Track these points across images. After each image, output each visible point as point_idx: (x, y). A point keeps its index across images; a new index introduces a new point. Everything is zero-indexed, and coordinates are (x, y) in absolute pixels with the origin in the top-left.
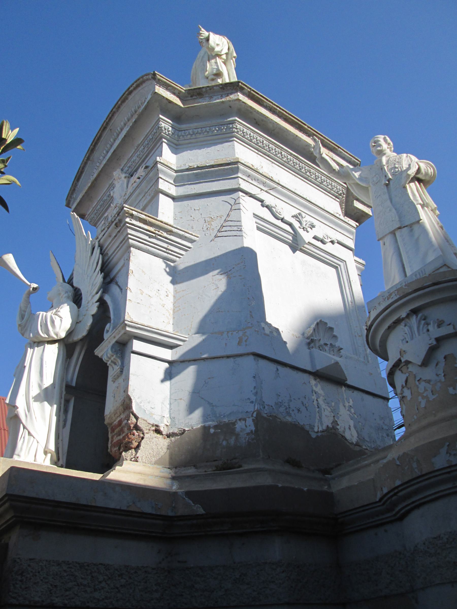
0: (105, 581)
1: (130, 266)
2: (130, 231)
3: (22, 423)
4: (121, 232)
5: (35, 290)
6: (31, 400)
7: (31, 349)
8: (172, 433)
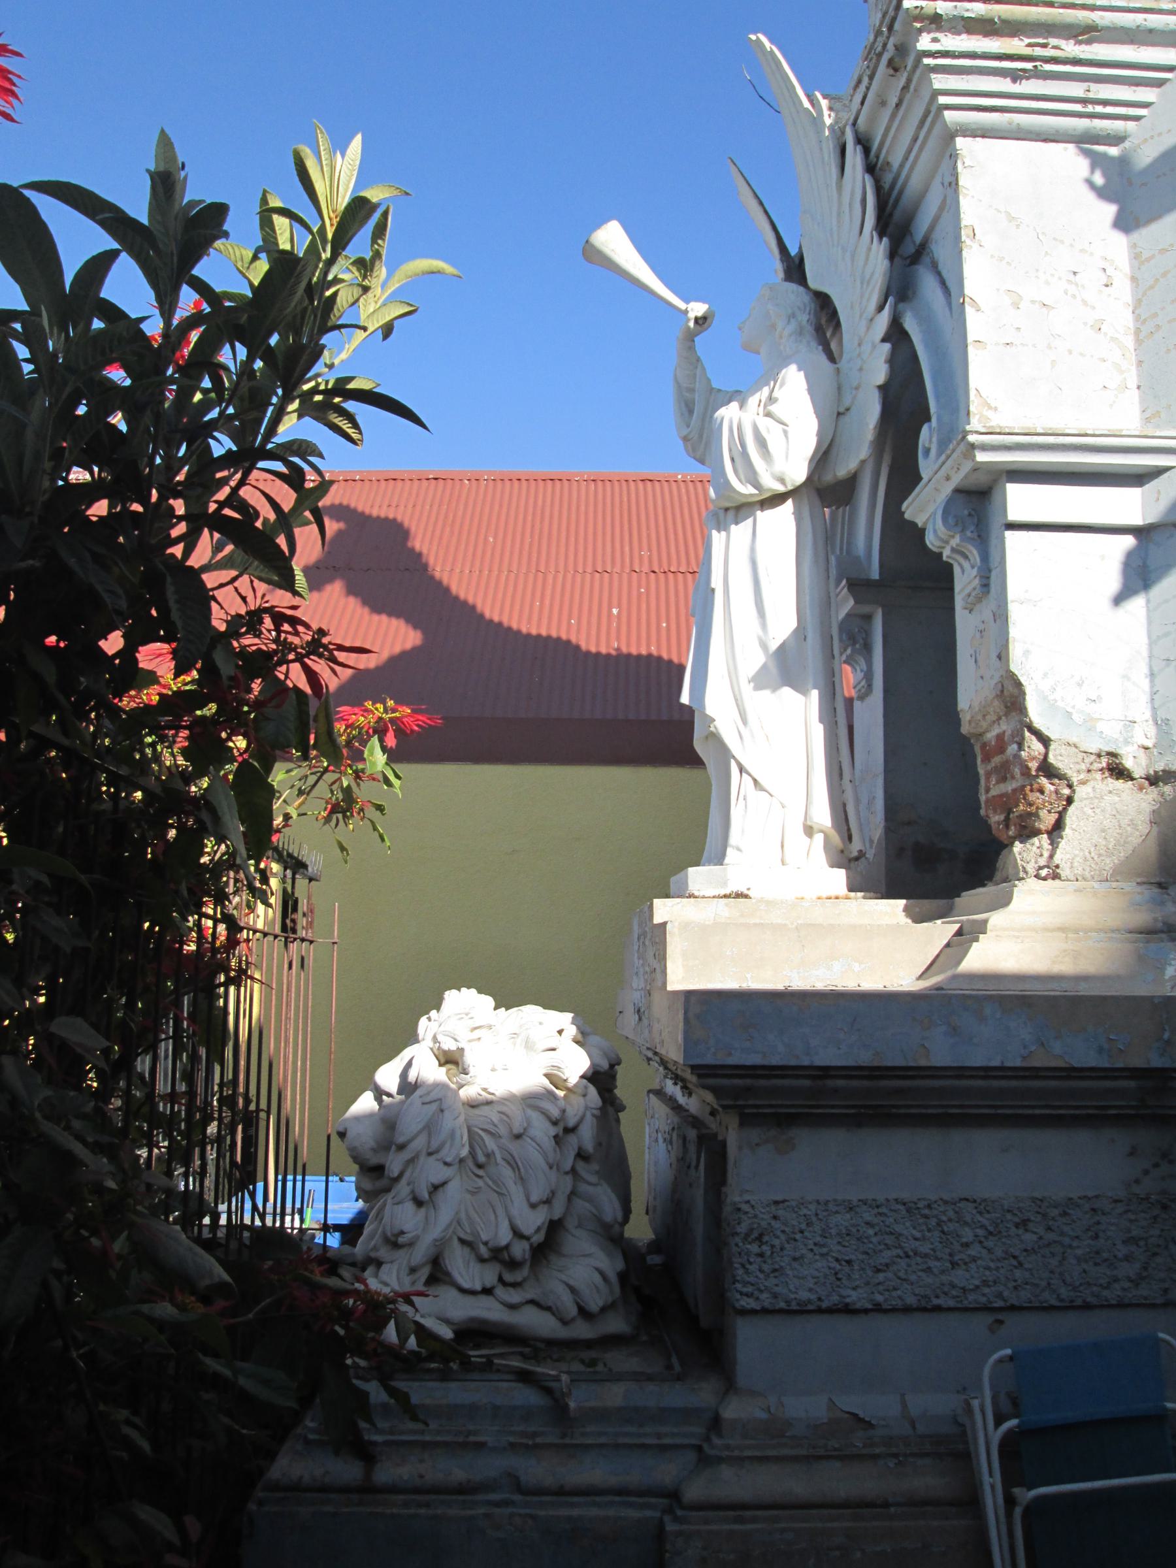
0: (981, 1242)
1: (962, 211)
2: (939, 82)
3: (734, 757)
4: (912, 87)
5: (704, 323)
6: (747, 689)
7: (719, 531)
8: (1163, 771)
